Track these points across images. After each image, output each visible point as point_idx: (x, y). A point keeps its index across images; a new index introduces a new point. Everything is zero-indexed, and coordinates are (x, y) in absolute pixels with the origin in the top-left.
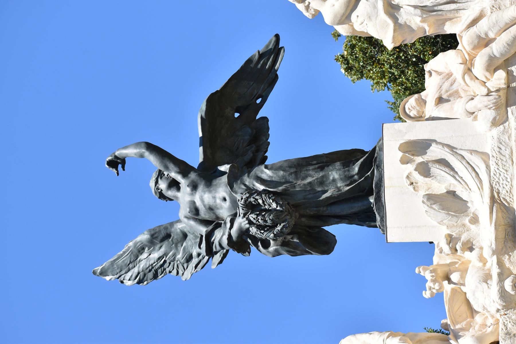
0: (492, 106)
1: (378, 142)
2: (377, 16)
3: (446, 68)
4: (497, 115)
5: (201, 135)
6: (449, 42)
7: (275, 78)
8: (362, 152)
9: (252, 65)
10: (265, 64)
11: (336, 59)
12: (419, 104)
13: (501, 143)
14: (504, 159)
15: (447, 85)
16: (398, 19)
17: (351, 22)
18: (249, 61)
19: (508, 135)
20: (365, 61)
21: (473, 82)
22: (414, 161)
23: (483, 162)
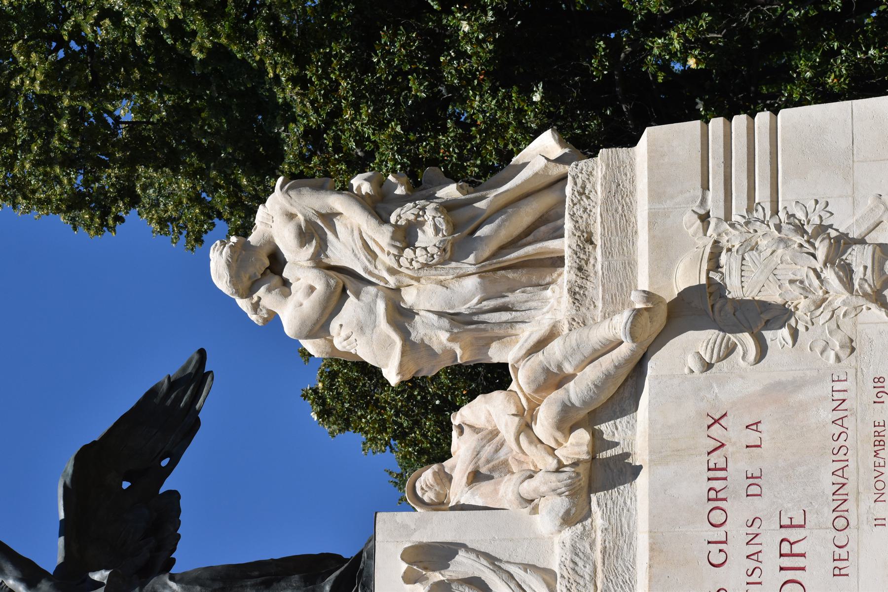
0: (563, 489)
1: (367, 544)
2: (375, 327)
3: (488, 421)
4: (573, 506)
5: (62, 515)
6: (496, 377)
7: (196, 425)
8: (337, 559)
9: (157, 401)
10: (179, 399)
11: (303, 396)
12: (439, 481)
13: (577, 555)
14: (582, 583)
15: (488, 449)
16: (409, 334)
17: (329, 334)
18: (152, 393)
19: (589, 540)
20: (354, 400)
21: (533, 448)
22: (427, 579)
23: (545, 586)
